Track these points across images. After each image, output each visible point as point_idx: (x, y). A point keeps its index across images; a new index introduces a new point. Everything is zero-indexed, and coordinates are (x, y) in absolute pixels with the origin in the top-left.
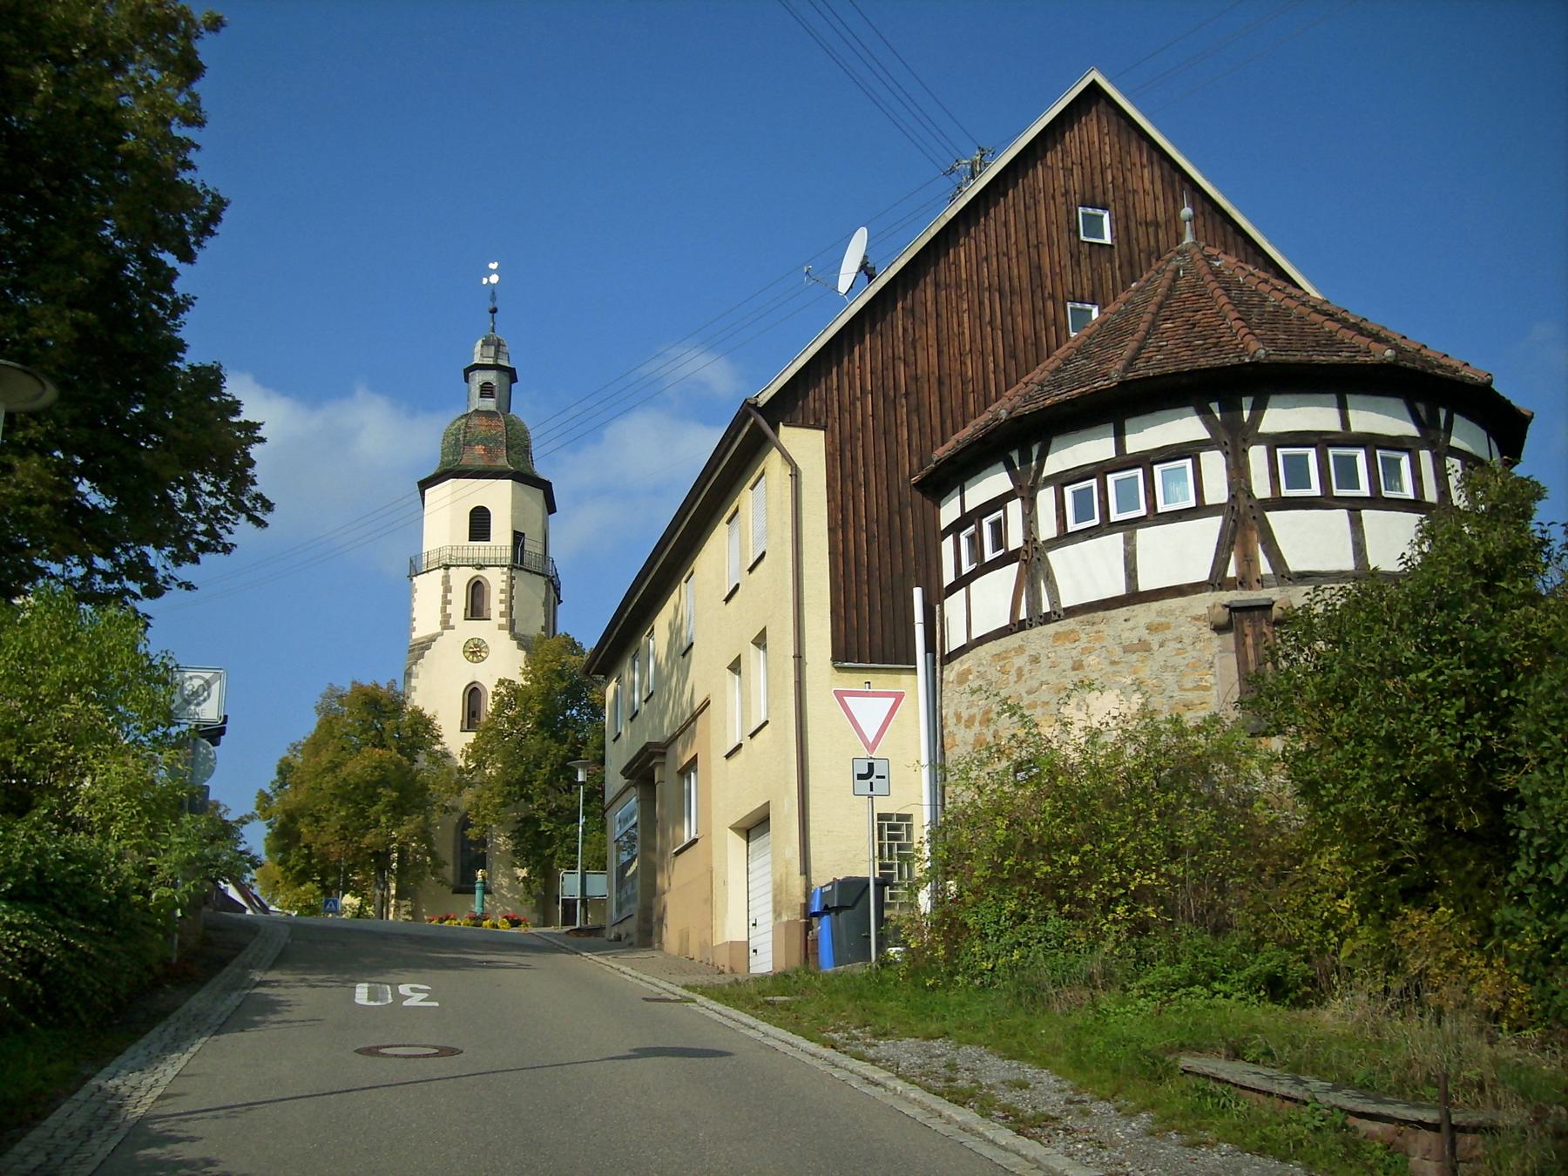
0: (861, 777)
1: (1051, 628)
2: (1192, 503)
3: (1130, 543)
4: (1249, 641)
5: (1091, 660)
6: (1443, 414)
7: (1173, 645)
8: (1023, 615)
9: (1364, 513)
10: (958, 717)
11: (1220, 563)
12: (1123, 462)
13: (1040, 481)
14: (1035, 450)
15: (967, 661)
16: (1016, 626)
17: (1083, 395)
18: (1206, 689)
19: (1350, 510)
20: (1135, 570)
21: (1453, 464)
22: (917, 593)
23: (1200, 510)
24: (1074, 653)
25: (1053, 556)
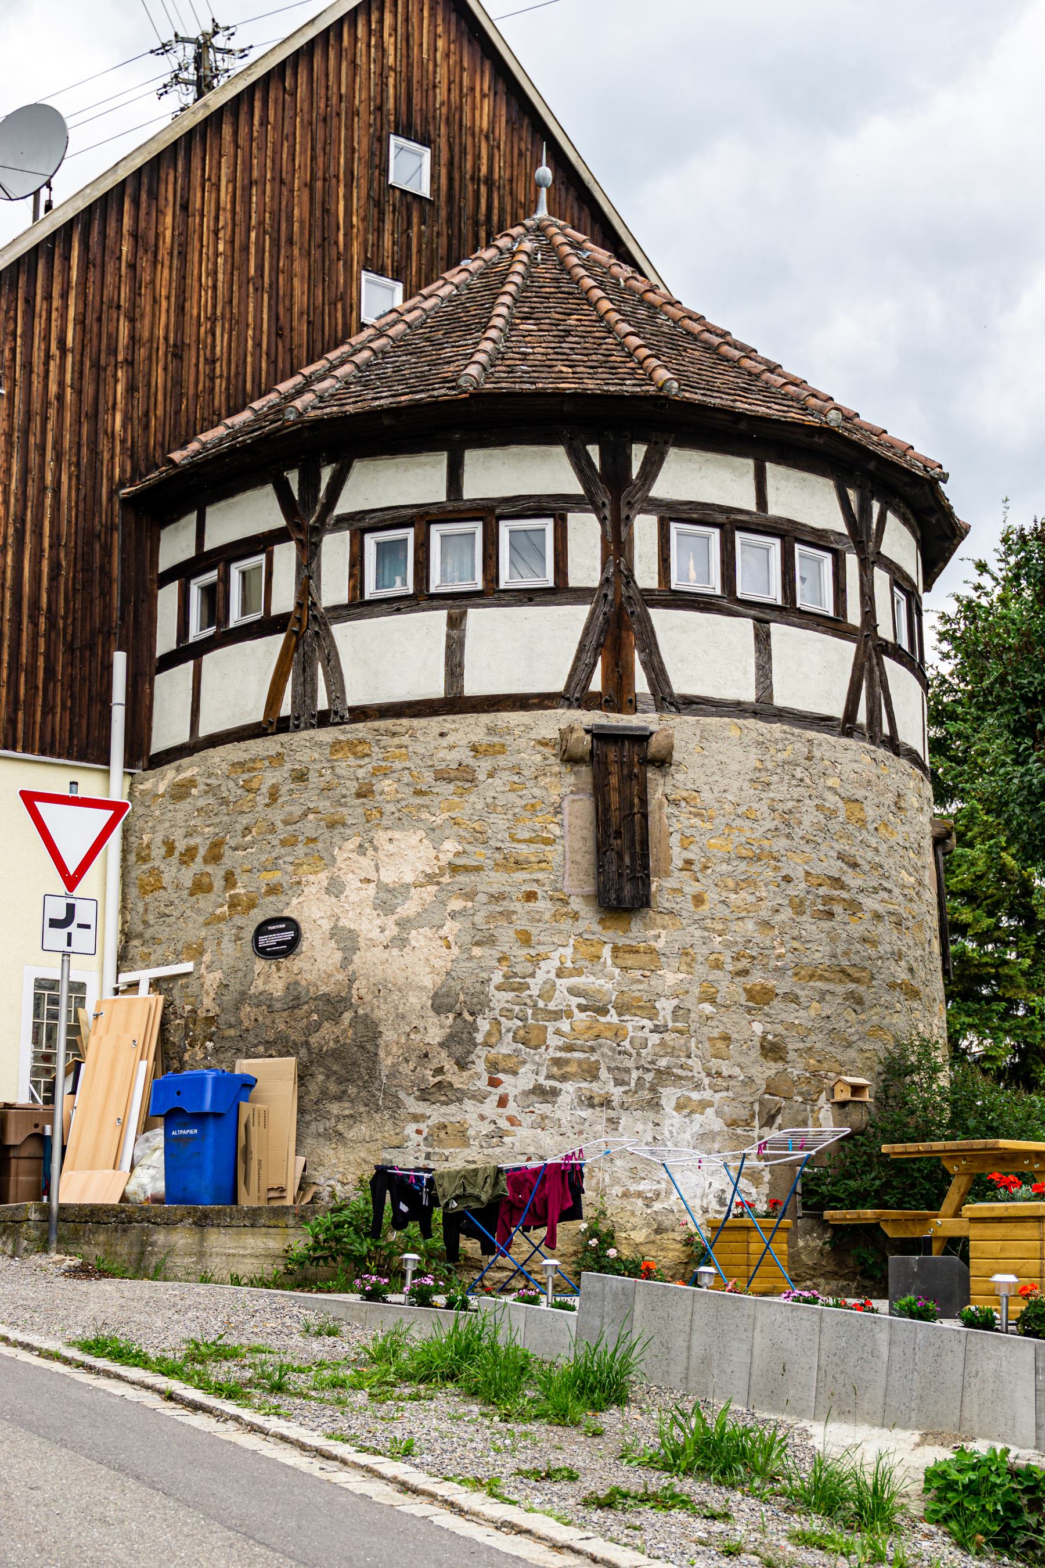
0: (54, 923)
1: (326, 735)
2: (549, 580)
3: (455, 623)
4: (614, 780)
5: (386, 785)
6: (876, 507)
7: (506, 776)
8: (286, 709)
9: (774, 627)
10: (170, 848)
11: (580, 672)
12: (455, 509)
13: (330, 520)
14: (326, 474)
15: (190, 768)
16: (273, 725)
17: (417, 405)
18: (547, 842)
19: (757, 619)
20: (461, 665)
21: (881, 578)
22: (120, 660)
23: (561, 592)
24: (361, 773)
25: (338, 630)
